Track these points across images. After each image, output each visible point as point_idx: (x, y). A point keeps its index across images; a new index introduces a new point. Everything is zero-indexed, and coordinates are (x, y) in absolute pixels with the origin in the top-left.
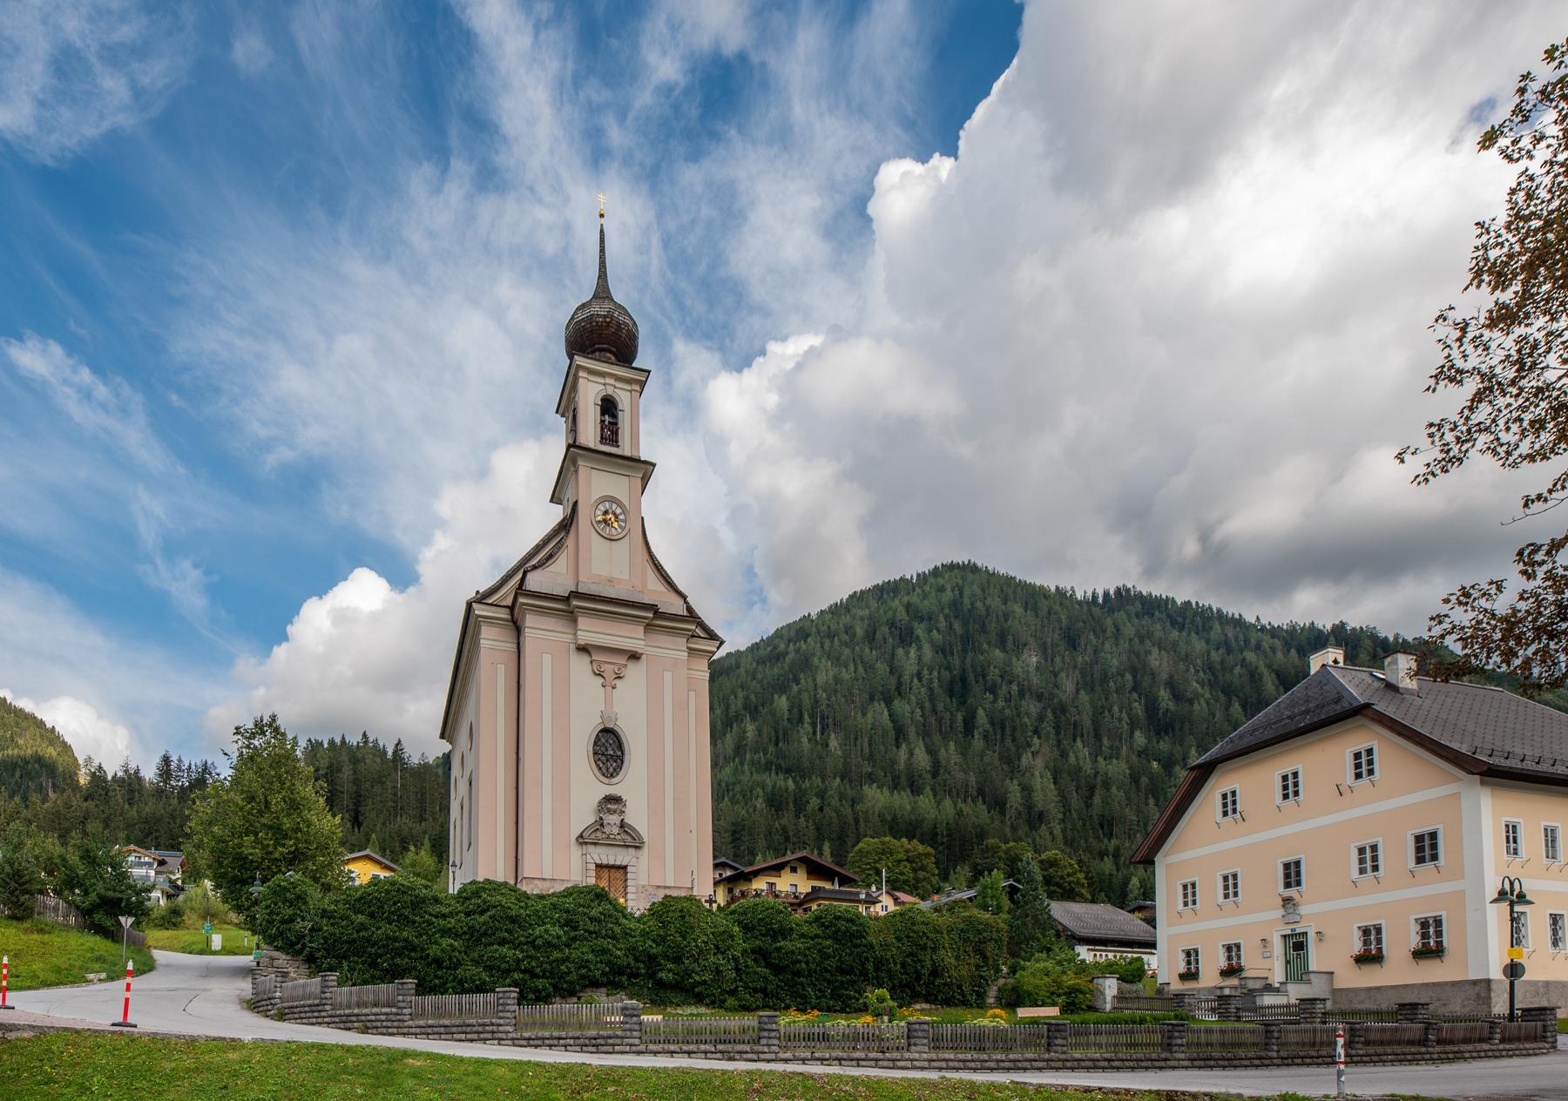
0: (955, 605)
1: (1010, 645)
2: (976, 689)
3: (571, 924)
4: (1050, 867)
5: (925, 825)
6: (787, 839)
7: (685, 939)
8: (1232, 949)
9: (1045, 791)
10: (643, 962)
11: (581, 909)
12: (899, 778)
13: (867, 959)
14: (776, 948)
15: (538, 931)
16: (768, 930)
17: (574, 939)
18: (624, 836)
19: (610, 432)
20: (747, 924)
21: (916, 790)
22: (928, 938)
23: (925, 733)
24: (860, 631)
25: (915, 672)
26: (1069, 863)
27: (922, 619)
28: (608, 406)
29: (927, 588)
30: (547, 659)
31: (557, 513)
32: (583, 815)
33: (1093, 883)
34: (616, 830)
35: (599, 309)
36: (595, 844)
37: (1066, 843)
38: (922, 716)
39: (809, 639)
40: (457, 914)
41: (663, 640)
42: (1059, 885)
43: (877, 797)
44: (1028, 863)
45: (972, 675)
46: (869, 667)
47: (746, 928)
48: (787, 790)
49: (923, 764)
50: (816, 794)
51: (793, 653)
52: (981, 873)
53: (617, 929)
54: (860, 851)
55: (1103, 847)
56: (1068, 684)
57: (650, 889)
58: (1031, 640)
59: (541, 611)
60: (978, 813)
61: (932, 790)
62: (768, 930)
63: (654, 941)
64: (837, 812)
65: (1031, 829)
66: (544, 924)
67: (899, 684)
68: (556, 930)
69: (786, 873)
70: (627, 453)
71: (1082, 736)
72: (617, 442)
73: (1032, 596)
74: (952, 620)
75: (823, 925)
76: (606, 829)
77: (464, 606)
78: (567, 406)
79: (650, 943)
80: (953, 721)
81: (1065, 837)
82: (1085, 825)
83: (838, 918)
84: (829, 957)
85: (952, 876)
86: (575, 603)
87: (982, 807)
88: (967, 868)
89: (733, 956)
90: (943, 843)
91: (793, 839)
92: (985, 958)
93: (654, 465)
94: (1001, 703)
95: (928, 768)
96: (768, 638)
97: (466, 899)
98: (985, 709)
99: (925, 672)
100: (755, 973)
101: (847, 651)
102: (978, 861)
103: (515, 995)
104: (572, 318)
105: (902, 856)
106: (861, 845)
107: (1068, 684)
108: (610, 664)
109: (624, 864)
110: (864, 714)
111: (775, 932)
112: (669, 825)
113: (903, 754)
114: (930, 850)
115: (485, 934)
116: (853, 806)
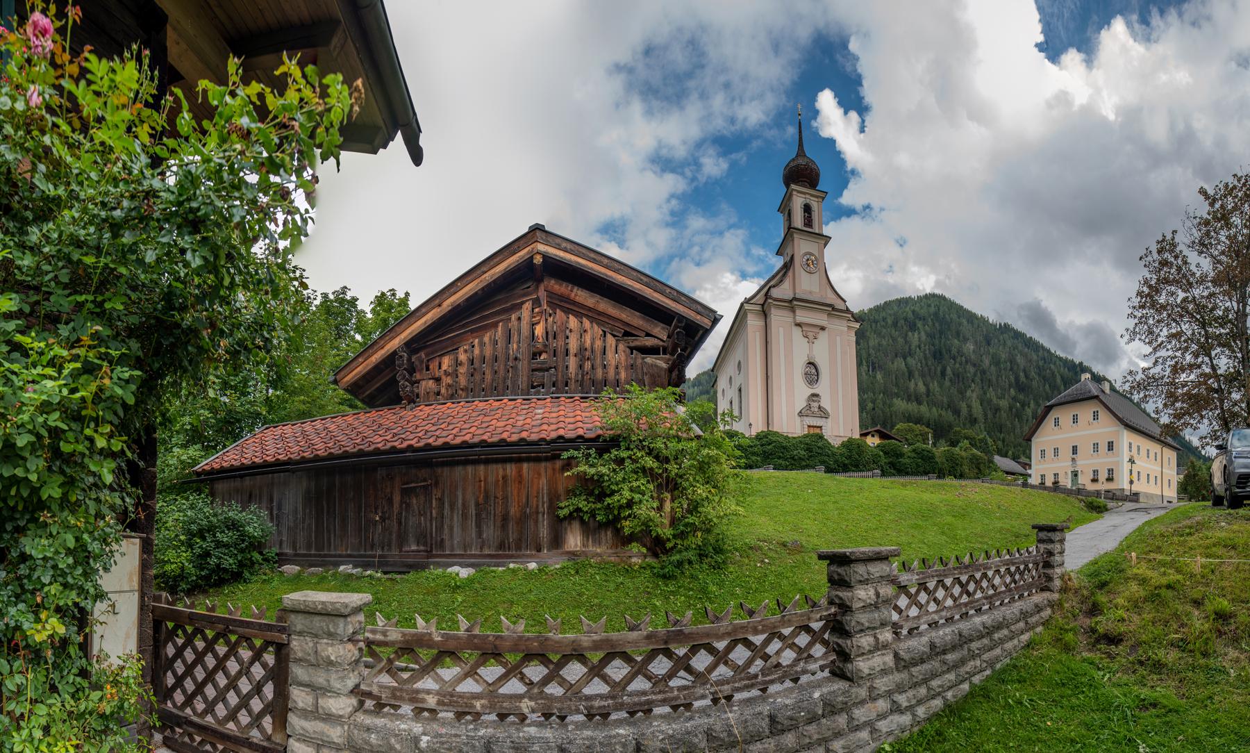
0: (936, 314)
1: (961, 338)
3: (809, 450)
8: (1056, 475)
9: (977, 410)
15: (795, 452)
17: (811, 456)
19: (808, 221)
21: (920, 403)
23: (923, 376)
27: (920, 319)
28: (807, 209)
30: (781, 329)
32: (801, 404)
35: (801, 161)
41: (837, 321)
43: (900, 405)
46: (894, 340)
47: (885, 453)
56: (987, 362)
59: (778, 307)
60: (948, 416)
68: (803, 453)
70: (817, 231)
73: (971, 317)
78: (785, 208)
80: (936, 369)
87: (950, 413)
94: (957, 365)
101: (884, 330)
104: (788, 165)
105: (918, 432)
106: (898, 426)
107: (987, 362)
113: (912, 385)
115: (771, 454)
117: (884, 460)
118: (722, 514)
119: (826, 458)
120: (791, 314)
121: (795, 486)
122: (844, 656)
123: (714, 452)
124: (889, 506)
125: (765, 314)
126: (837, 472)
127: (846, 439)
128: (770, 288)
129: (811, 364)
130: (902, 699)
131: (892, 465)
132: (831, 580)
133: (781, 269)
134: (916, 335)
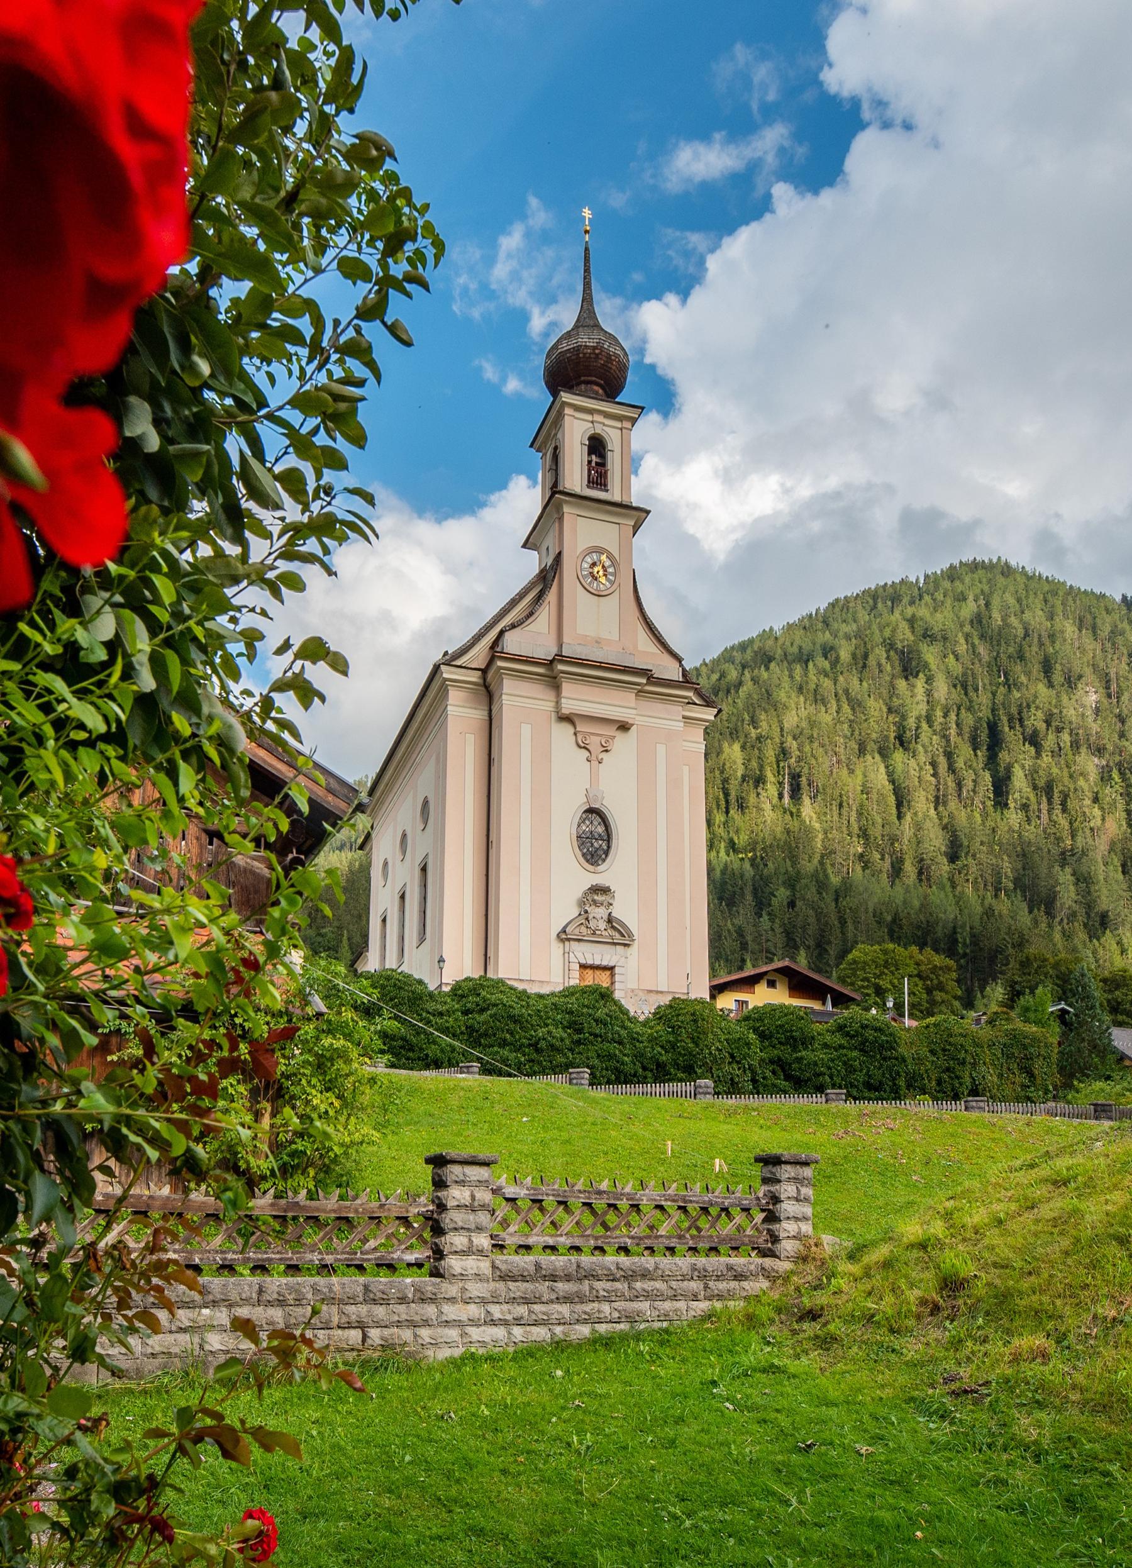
1: (1058, 678)
2: (1011, 736)
3: (575, 1026)
4: (1116, 989)
5: (939, 929)
6: (744, 946)
7: (697, 1045)
10: (651, 1071)
11: (585, 1010)
13: (898, 1074)
14: (797, 1058)
16: (787, 1038)
17: (578, 1042)
18: (611, 932)
19: (598, 476)
20: (763, 1031)
22: (966, 1051)
24: (845, 655)
25: (924, 713)
28: (596, 446)
29: (939, 596)
30: (526, 730)
31: (531, 564)
32: (565, 911)
34: (602, 925)
35: (586, 340)
36: (579, 940)
38: (933, 775)
39: (772, 665)
40: (454, 1012)
44: (1083, 975)
45: (1005, 719)
47: (762, 1036)
48: (742, 876)
50: (784, 883)
51: (750, 683)
53: (623, 1033)
54: (855, 962)
57: (641, 993)
58: (1088, 671)
62: (787, 1038)
63: (662, 1047)
64: (819, 915)
66: (547, 1025)
68: (559, 1032)
70: (617, 498)
72: (605, 485)
74: (977, 641)
75: (848, 1034)
76: (592, 924)
77: (431, 668)
79: (659, 1049)
83: (864, 1027)
84: (855, 1071)
85: (979, 1002)
86: (561, 667)
89: (750, 1066)
90: (965, 955)
91: (752, 946)
92: (1031, 1075)
93: (648, 512)
97: (463, 996)
98: (1023, 767)
99: (939, 713)
100: (774, 1085)
101: (827, 683)
102: (1017, 978)
103: (587, 1076)
108: (595, 735)
109: (611, 964)
110: (852, 772)
111: (795, 1040)
114: (951, 963)
115: (486, 1035)
116: (837, 900)
117: (757, 1053)
118: (347, 1140)
119: (615, 1049)
120: (551, 695)
121: (498, 1109)
122: (439, 1254)
123: (340, 1043)
126: (643, 1081)
127: (665, 1000)
128: (501, 633)
129: (593, 812)
130: (496, 1311)
131: (781, 1066)
134: (920, 684)
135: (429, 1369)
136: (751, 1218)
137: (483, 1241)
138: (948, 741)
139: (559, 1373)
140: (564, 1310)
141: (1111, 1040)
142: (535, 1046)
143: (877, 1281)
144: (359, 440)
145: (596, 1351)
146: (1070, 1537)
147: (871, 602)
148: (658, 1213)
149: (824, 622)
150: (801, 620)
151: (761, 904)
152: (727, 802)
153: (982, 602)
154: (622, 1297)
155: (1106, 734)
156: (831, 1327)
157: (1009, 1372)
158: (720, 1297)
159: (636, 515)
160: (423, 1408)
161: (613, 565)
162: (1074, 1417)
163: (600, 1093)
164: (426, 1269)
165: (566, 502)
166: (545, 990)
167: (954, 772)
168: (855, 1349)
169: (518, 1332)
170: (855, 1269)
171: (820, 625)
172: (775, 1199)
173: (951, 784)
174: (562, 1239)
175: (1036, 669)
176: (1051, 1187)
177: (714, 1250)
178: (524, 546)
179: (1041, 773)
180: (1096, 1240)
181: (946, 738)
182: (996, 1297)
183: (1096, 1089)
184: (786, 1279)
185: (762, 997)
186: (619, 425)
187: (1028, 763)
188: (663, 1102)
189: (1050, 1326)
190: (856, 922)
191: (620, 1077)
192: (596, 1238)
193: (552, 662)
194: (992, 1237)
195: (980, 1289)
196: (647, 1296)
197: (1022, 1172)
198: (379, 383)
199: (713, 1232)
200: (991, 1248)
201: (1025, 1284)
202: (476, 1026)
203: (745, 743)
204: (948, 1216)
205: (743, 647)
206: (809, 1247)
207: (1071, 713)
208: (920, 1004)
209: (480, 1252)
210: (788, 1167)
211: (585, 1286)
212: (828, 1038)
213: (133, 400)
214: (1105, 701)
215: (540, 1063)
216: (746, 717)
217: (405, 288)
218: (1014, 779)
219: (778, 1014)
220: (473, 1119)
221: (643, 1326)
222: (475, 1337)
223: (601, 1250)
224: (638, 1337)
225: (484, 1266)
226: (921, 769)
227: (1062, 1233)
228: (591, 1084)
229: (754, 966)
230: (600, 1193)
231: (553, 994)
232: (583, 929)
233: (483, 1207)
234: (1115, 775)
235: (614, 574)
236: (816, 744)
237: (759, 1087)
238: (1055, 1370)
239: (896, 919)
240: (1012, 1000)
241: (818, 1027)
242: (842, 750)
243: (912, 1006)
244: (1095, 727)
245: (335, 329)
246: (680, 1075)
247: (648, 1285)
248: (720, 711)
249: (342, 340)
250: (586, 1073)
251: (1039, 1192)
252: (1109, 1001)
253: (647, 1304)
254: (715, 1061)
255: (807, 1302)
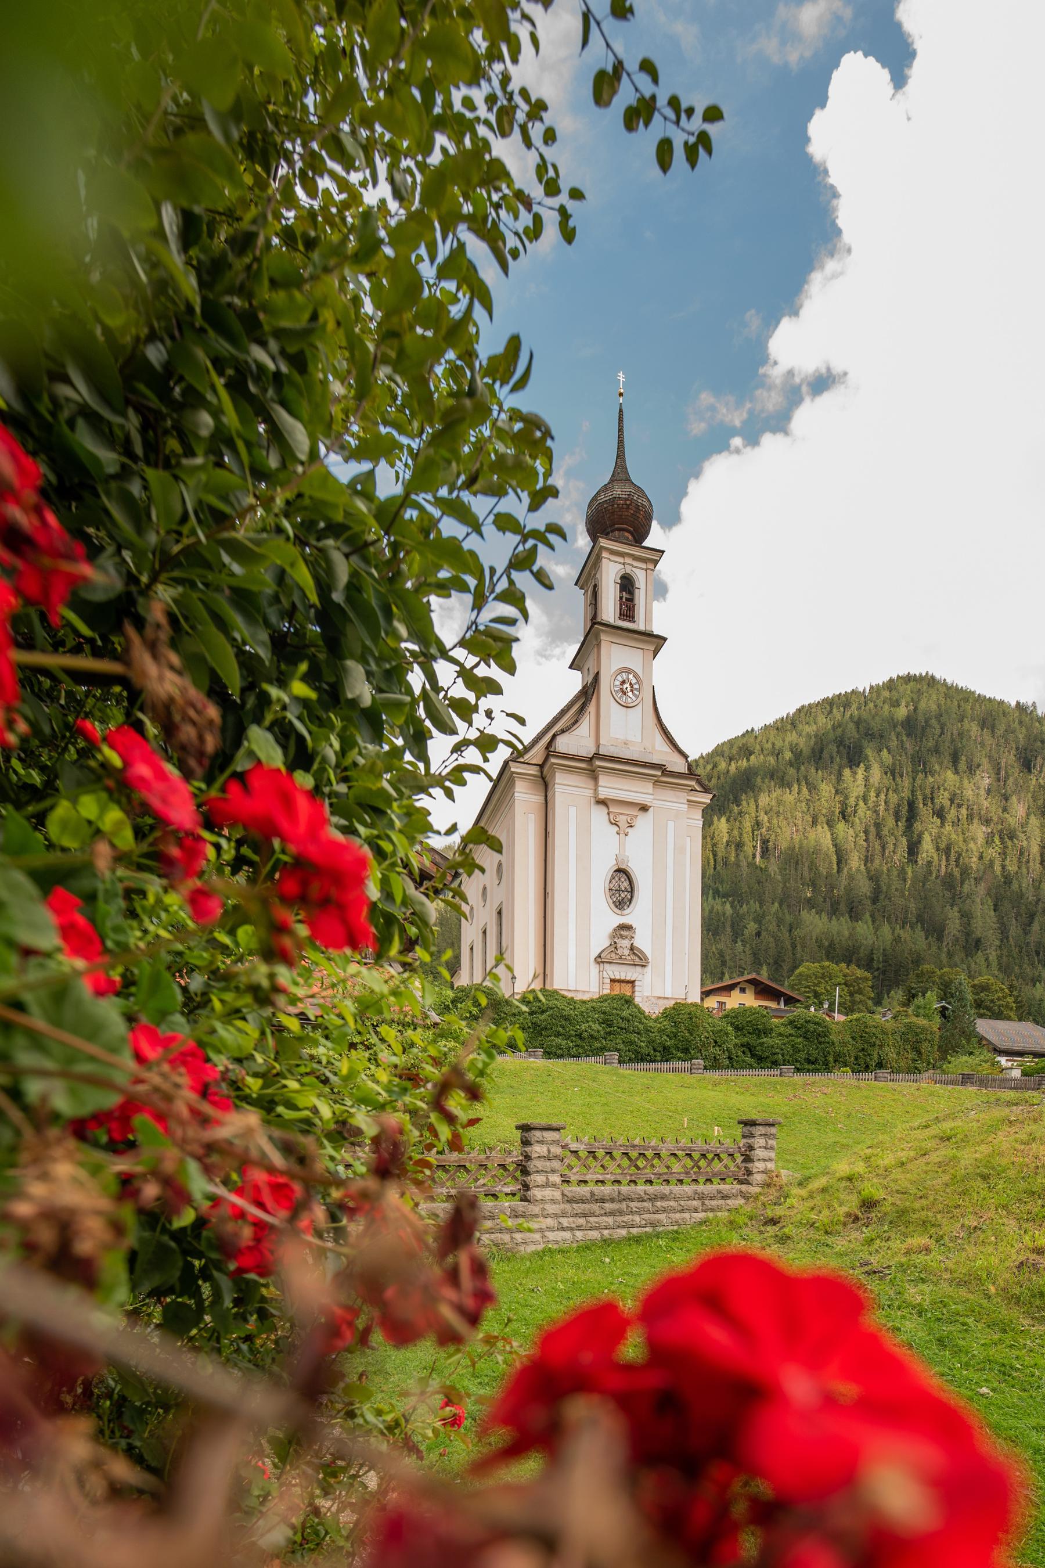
1: (962, 766)
2: (924, 811)
5: (862, 950)
6: (724, 963)
12: (838, 903)
13: (829, 1053)
15: (584, 1027)
17: (610, 1033)
19: (628, 610)
21: (854, 915)
25: (861, 794)
26: (999, 985)
28: (627, 584)
30: (573, 811)
32: (600, 941)
33: (1021, 1007)
34: (627, 952)
35: (619, 491)
37: (999, 969)
38: (865, 841)
41: (669, 795)
42: (988, 1009)
44: (960, 984)
45: (920, 798)
47: (737, 1028)
48: (724, 914)
49: (864, 890)
52: (914, 996)
53: (641, 1027)
54: (800, 974)
55: (1037, 974)
58: (985, 761)
59: (569, 769)
60: (916, 939)
61: (871, 916)
64: (777, 940)
65: (967, 956)
67: (844, 805)
68: (596, 1027)
69: (736, 993)
70: (642, 627)
71: (1028, 861)
72: (633, 617)
74: (904, 738)
75: (796, 1027)
76: (619, 951)
81: (999, 964)
82: (1020, 952)
83: (807, 1022)
86: (598, 763)
87: (920, 934)
88: (901, 993)
90: (878, 969)
91: (729, 963)
92: (919, 1053)
93: (665, 639)
95: (868, 894)
96: (708, 755)
98: (931, 834)
99: (873, 794)
100: (744, 1061)
101: (792, 771)
102: (913, 985)
104: (595, 498)
105: (840, 980)
106: (801, 969)
112: (669, 948)
114: (868, 975)
116: (790, 931)
117: (733, 1040)
119: (634, 1037)
120: (590, 784)
121: (558, 1082)
122: (526, 1187)
124: (676, 1111)
125: (544, 782)
128: (554, 736)
130: (565, 1222)
131: (749, 1048)
132: (522, 1142)
133: (577, 698)
134: (861, 771)
135: (522, 1259)
136: (734, 1160)
137: (556, 1179)
138: (878, 815)
139: (607, 1260)
140: (610, 1220)
141: (975, 1028)
142: (580, 1036)
143: (818, 1200)
144: (510, 668)
145: (630, 1245)
146: (941, 1362)
147: (828, 708)
148: (673, 1158)
149: (792, 724)
150: (775, 723)
151: (737, 934)
152: (715, 860)
153: (911, 708)
154: (648, 1212)
155: (993, 809)
156: (786, 1230)
157: (904, 1260)
158: (712, 1210)
159: (657, 642)
160: (520, 1284)
161: (638, 682)
162: (945, 1288)
163: (625, 1071)
164: (517, 1197)
165: (603, 631)
166: (586, 997)
167: (880, 838)
168: (802, 1244)
169: (579, 1234)
170: (803, 1192)
171: (789, 727)
172: (751, 1148)
173: (878, 847)
174: (608, 1176)
175: (947, 760)
176: (938, 1141)
177: (709, 1180)
178: (571, 667)
179: (943, 838)
180: (966, 1178)
181: (876, 812)
182: (897, 1212)
183: (961, 1063)
184: (756, 1198)
185: (735, 1001)
186: (644, 566)
187: (934, 831)
188: (670, 1076)
189: (933, 1231)
190: (804, 947)
191: (640, 1058)
192: (631, 1175)
193: (591, 759)
194: (897, 1174)
195: (887, 1207)
196: (664, 1210)
197: (919, 1131)
198: (526, 622)
199: (708, 1169)
200: (896, 1181)
201: (917, 1205)
202: (539, 1023)
203: (729, 817)
204: (867, 1159)
205: (731, 743)
206: (772, 1178)
207: (969, 793)
208: (844, 1003)
209: (554, 1186)
210: (761, 1128)
211: (624, 1205)
212: (782, 1029)
213: (350, 663)
214: (995, 784)
215: (583, 1047)
216: (731, 797)
217: (546, 538)
218: (923, 843)
219: (748, 1013)
220: (540, 1089)
221: (661, 1229)
222: (551, 1238)
223: (635, 1182)
224: (658, 1236)
225: (557, 1194)
226: (857, 836)
227: (944, 1172)
228: (620, 1062)
229: (731, 978)
230: (634, 1146)
231: (592, 1000)
232: (613, 955)
233: (556, 1157)
234: (997, 840)
235: (639, 690)
236: (781, 818)
237: (733, 1063)
238: (934, 1259)
239: (832, 945)
240: (909, 1001)
241: (775, 1021)
242: (800, 822)
243: (840, 1004)
244: (986, 804)
245: (491, 578)
246: (680, 1055)
247: (665, 1204)
248: (714, 796)
249: (499, 589)
250: (616, 1055)
251: (930, 1145)
252: (975, 1000)
253: (664, 1215)
254: (703, 1045)
255: (770, 1214)
